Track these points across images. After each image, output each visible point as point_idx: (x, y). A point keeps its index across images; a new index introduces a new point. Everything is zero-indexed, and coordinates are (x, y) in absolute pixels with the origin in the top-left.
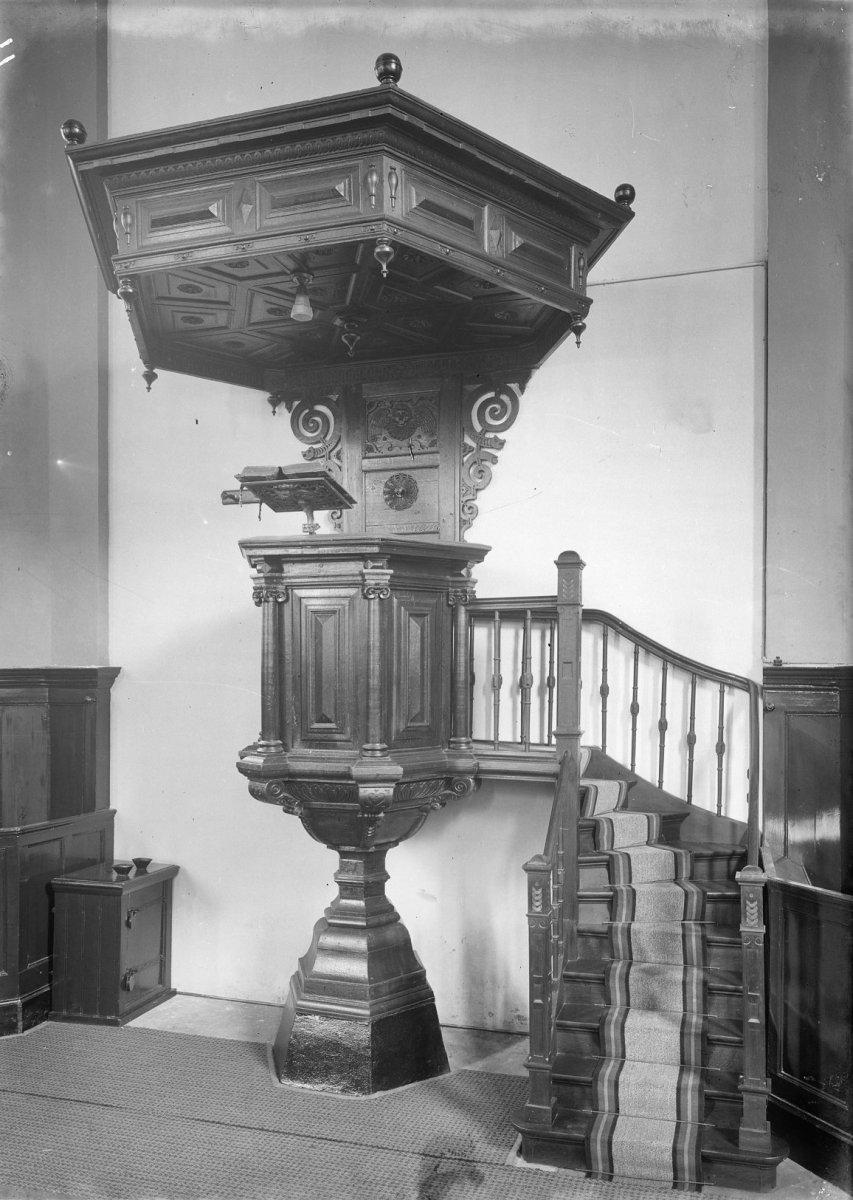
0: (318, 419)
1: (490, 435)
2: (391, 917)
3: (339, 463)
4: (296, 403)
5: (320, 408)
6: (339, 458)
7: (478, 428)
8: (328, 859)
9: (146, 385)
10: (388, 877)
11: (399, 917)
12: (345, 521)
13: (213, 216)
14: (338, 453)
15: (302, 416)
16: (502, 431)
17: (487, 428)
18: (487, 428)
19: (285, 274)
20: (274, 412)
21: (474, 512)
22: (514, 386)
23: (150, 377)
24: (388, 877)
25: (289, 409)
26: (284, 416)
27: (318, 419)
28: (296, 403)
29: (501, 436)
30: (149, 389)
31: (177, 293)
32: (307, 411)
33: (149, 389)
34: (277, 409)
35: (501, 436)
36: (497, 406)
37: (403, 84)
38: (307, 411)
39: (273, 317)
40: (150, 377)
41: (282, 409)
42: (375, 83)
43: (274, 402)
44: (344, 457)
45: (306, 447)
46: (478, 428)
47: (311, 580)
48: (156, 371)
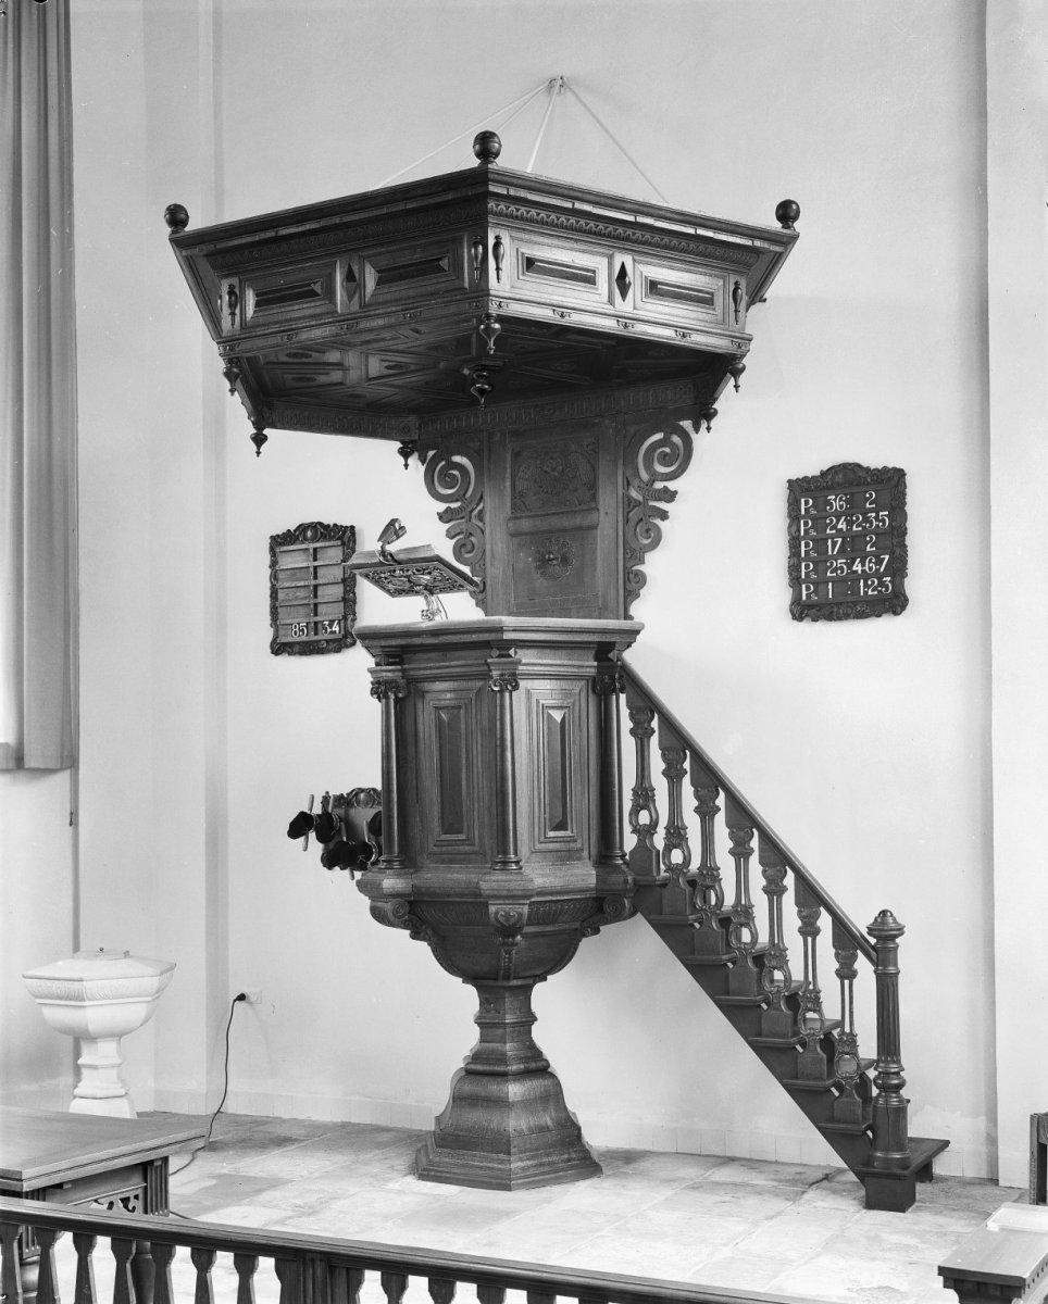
0: (456, 472)
1: (659, 485)
2: (540, 1064)
3: (480, 524)
4: (431, 453)
5: (457, 459)
6: (481, 520)
7: (645, 476)
8: (466, 998)
9: (255, 448)
10: (536, 1019)
11: (549, 1066)
12: (489, 597)
13: (318, 295)
14: (481, 512)
15: (438, 469)
16: (671, 479)
17: (655, 477)
18: (655, 477)
19: (146, 1188)
20: (406, 466)
21: (641, 579)
22: (687, 424)
23: (259, 440)
24: (536, 1019)
25: (423, 460)
26: (417, 467)
27: (456, 472)
28: (431, 453)
29: (672, 485)
30: (258, 453)
31: (286, 359)
32: (443, 463)
33: (258, 453)
34: (410, 461)
35: (672, 485)
36: (667, 450)
37: (502, 163)
38: (443, 463)
39: (392, 372)
40: (259, 440)
41: (413, 460)
42: (475, 162)
43: (405, 453)
44: (487, 518)
45: (442, 507)
46: (645, 476)
47: (542, 668)
48: (267, 431)
